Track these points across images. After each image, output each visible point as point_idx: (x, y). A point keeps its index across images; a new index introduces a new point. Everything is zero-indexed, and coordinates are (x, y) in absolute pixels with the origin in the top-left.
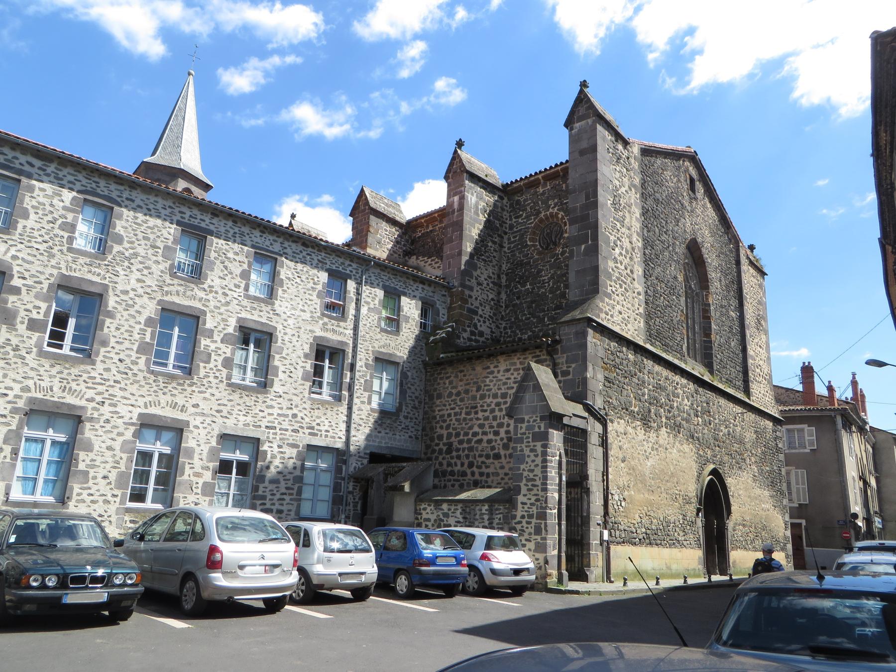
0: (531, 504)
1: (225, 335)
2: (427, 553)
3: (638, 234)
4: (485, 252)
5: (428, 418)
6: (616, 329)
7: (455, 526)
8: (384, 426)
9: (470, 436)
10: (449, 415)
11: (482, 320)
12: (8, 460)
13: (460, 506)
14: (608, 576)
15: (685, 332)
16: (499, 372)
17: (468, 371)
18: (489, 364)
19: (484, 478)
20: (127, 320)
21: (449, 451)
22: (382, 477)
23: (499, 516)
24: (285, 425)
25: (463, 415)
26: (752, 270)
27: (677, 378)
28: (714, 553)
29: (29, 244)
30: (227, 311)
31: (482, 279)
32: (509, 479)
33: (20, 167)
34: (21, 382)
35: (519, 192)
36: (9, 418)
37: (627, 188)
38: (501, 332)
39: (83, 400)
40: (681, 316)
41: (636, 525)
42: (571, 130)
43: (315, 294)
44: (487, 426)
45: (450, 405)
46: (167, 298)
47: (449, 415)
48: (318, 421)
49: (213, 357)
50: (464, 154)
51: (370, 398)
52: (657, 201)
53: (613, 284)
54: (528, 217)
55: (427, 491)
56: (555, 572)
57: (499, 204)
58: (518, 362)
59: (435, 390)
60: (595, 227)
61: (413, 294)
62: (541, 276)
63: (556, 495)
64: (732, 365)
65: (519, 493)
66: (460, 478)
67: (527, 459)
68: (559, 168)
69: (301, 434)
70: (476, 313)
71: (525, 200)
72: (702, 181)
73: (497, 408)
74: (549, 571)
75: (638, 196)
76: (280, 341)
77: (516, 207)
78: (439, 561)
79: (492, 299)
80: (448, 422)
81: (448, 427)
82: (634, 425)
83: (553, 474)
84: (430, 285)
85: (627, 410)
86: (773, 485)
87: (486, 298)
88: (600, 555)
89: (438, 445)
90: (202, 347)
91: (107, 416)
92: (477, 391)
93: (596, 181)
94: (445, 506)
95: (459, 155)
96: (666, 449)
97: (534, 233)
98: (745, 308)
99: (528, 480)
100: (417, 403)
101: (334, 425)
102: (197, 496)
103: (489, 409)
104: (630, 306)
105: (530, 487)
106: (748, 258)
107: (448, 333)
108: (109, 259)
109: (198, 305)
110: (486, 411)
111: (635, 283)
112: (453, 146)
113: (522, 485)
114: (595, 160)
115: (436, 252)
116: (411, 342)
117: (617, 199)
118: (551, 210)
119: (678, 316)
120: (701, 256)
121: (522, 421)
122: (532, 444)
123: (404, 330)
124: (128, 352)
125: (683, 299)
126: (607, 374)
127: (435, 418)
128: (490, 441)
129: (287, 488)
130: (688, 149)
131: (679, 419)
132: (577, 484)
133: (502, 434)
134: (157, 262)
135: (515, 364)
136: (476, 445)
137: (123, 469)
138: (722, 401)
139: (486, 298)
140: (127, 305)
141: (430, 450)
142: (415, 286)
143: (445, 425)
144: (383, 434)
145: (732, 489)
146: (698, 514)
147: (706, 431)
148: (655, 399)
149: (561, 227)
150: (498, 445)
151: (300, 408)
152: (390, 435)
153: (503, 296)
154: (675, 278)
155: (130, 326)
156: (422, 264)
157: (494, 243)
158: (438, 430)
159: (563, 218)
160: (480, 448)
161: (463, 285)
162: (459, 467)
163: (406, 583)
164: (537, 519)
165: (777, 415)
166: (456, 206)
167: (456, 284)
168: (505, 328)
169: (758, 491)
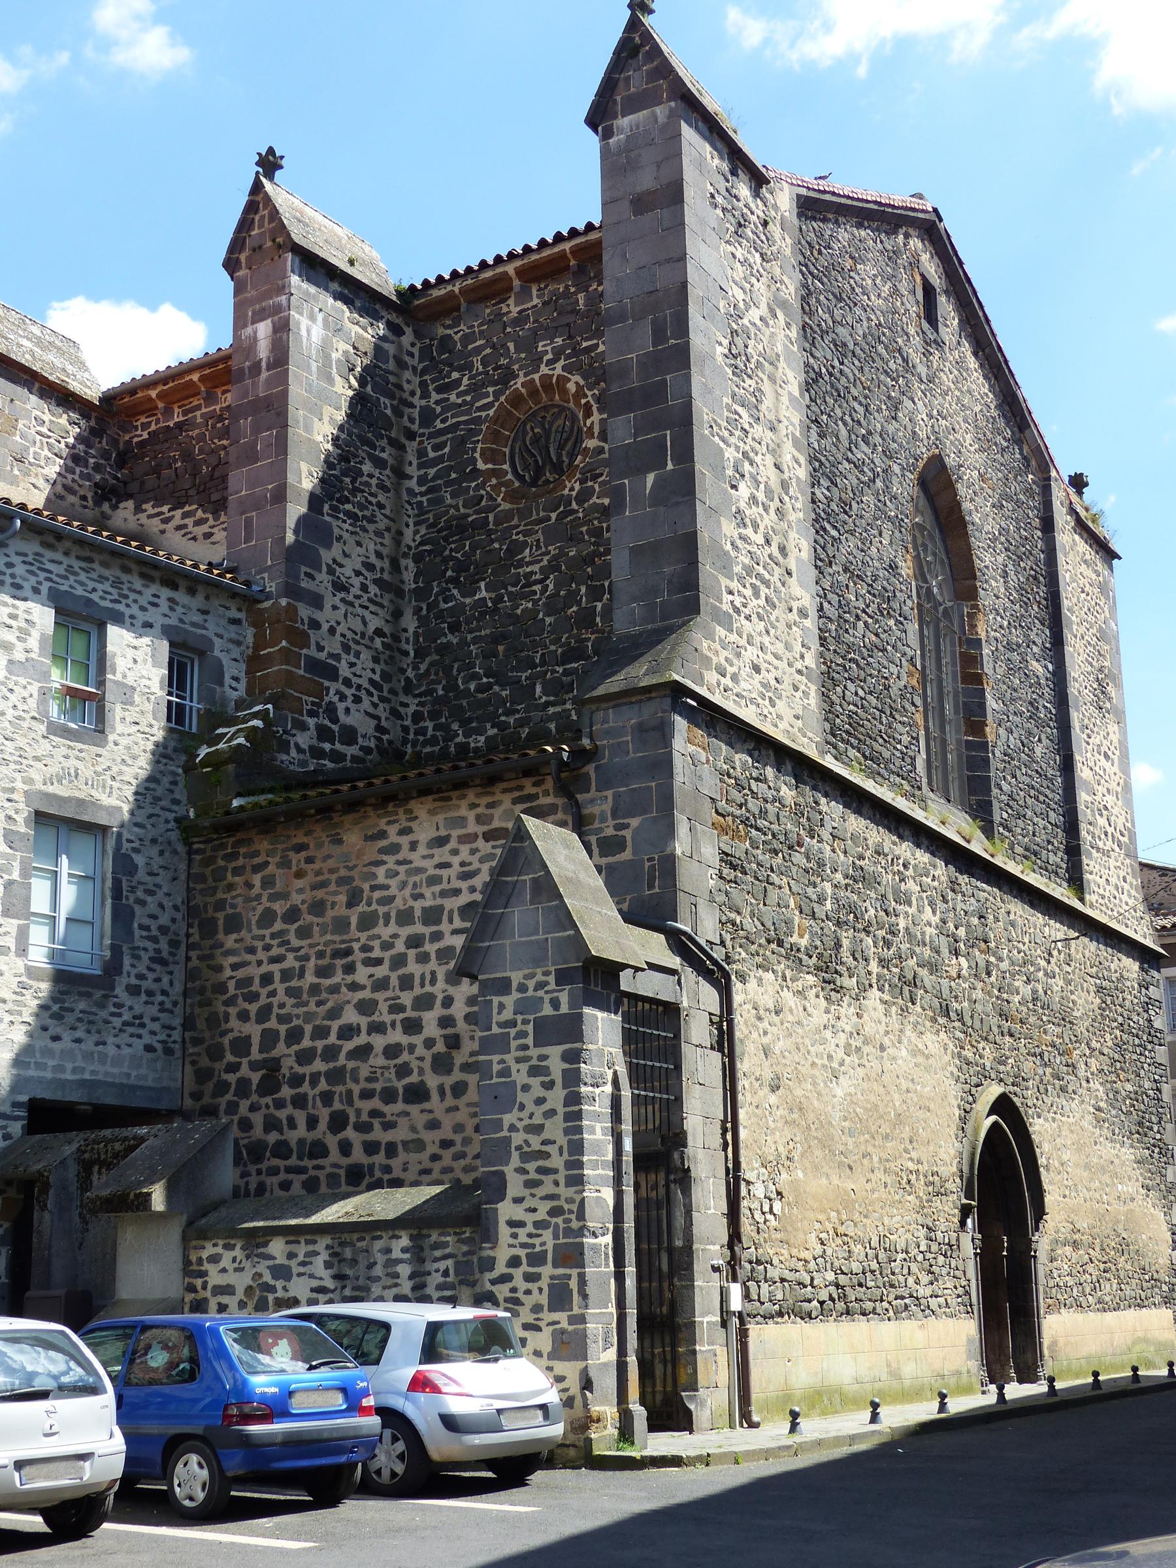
0: (537, 1224)
2: (261, 1384)
3: (796, 443)
4: (355, 491)
5: (202, 991)
6: (747, 714)
7: (312, 1302)
8: (70, 1018)
10: (267, 979)
11: (349, 692)
13: (322, 1243)
14: (744, 1411)
15: (919, 718)
16: (413, 846)
17: (320, 846)
18: (382, 824)
19: (380, 1159)
21: (270, 1085)
22: (73, 1170)
23: (442, 1265)
25: (310, 978)
26: (1082, 546)
27: (905, 850)
28: (1001, 1324)
31: (348, 572)
35: (447, 313)
37: (763, 310)
38: (405, 729)
40: (910, 674)
41: (812, 1265)
42: (606, 135)
44: (383, 1007)
45: (267, 948)
51: (23, 936)
52: (840, 347)
53: (735, 585)
54: (476, 389)
55: (216, 1206)
56: (608, 1411)
57: (390, 348)
58: (471, 816)
59: (220, 905)
60: (684, 421)
61: (142, 617)
63: (608, 1195)
64: (1040, 807)
65: (499, 1193)
66: (307, 1163)
67: (521, 1097)
68: (567, 246)
70: (333, 674)
71: (468, 339)
72: (954, 291)
73: (412, 953)
74: (595, 1409)
75: (794, 333)
77: (440, 360)
78: (298, 1405)
79: (379, 632)
80: (263, 1000)
81: (264, 1014)
82: (799, 985)
83: (599, 1135)
84: (192, 592)
85: (780, 943)
86: (1142, 1128)
87: (359, 627)
88: (721, 1352)
89: (233, 1068)
92: (350, 905)
93: (683, 287)
94: (277, 1247)
95: (268, 199)
96: (882, 1048)
97: (495, 436)
98: (1068, 650)
100: (164, 945)
103: (387, 955)
104: (779, 647)
105: (533, 1175)
106: (1072, 511)
107: (251, 733)
110: (378, 962)
111: (793, 581)
112: (251, 170)
113: (509, 1170)
114: (679, 225)
115: (207, 491)
116: (141, 767)
117: (739, 341)
118: (544, 370)
119: (901, 677)
120: (956, 506)
121: (504, 986)
122: (534, 1052)
123: (120, 728)
125: (913, 627)
126: (726, 843)
127: (221, 988)
128: (392, 1051)
130: (915, 203)
131: (912, 962)
132: (659, 1158)
133: (431, 1029)
135: (462, 822)
136: (351, 1065)
138: (1018, 909)
139: (359, 627)
141: (210, 1085)
142: (148, 593)
143: (253, 1008)
144: (66, 1043)
145: (1046, 1147)
146: (963, 1223)
147: (978, 994)
148: (852, 909)
149: (574, 419)
150: (420, 1059)
152: (88, 1045)
153: (410, 623)
154: (893, 567)
156: (155, 525)
157: (379, 463)
158: (234, 1023)
159: (580, 393)
160: (364, 1072)
161: (292, 590)
162: (301, 1131)
163: (204, 1474)
164: (555, 1265)
165: (1149, 943)
166: (263, 351)
167: (271, 587)
168: (417, 717)
169: (1107, 1150)
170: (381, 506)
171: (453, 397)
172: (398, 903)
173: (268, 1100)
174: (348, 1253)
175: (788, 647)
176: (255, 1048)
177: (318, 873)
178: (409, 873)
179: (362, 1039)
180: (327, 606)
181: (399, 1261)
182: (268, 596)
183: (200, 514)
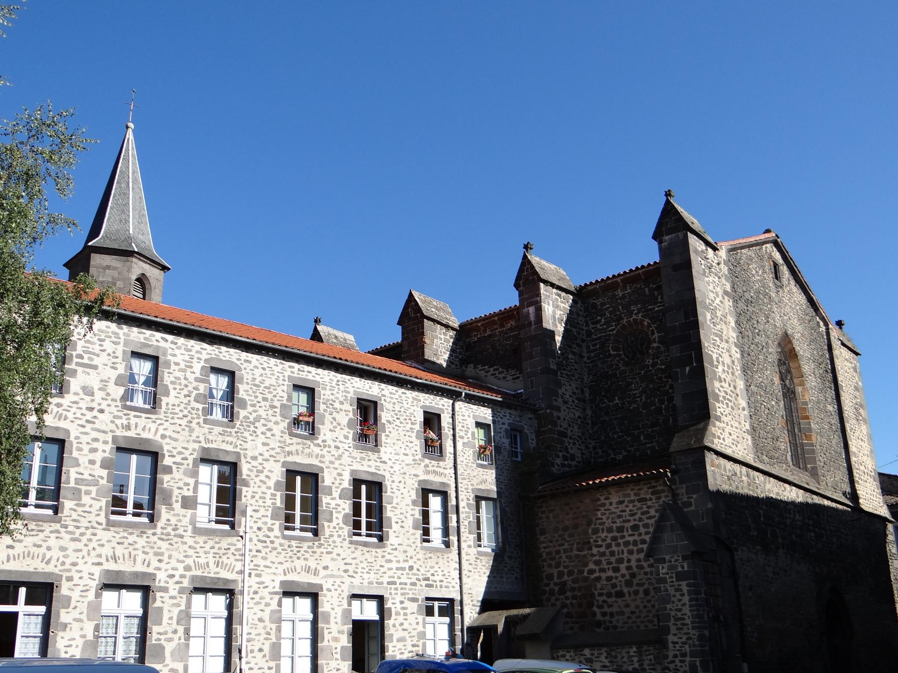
0: (682, 643)
1: (342, 490)
3: (736, 345)
9: (585, 574)
12: (183, 641)
16: (611, 504)
19: (607, 618)
20: (259, 487)
21: (562, 591)
23: (649, 657)
24: (404, 579)
29: (172, 421)
30: (341, 465)
32: (637, 618)
33: (157, 344)
34: (183, 562)
36: (179, 599)
39: (234, 572)
42: (660, 243)
43: (414, 435)
44: (604, 563)
45: (557, 541)
46: (290, 459)
47: (558, 552)
48: (432, 571)
49: (335, 515)
50: (534, 259)
54: (608, 323)
58: (632, 493)
62: (631, 390)
67: (673, 599)
68: (641, 271)
69: (418, 587)
71: (603, 304)
73: (613, 543)
75: (731, 304)
76: (389, 490)
79: (579, 417)
84: (516, 409)
89: (548, 585)
90: (324, 505)
91: (255, 587)
98: (842, 398)
99: (677, 619)
101: (447, 574)
102: (338, 662)
104: (736, 424)
105: (679, 626)
108: (237, 426)
109: (315, 462)
111: (739, 398)
113: (670, 624)
118: (634, 317)
121: (663, 561)
124: (264, 519)
127: (541, 555)
128: (609, 579)
129: (413, 646)
133: (623, 570)
134: (276, 423)
137: (274, 640)
140: (257, 471)
149: (647, 334)
151: (415, 559)
153: (589, 412)
155: (263, 493)
157: (574, 353)
158: (546, 568)
159: (649, 325)
167: (543, 405)
168: (594, 448)
170: (576, 370)
171: (598, 326)
172: (607, 525)
173: (562, 597)
174: (613, 653)
175: (740, 423)
176: (555, 578)
177: (575, 513)
178: (610, 514)
179: (597, 574)
180: (562, 410)
181: (633, 656)
182: (542, 409)
183: (500, 369)
